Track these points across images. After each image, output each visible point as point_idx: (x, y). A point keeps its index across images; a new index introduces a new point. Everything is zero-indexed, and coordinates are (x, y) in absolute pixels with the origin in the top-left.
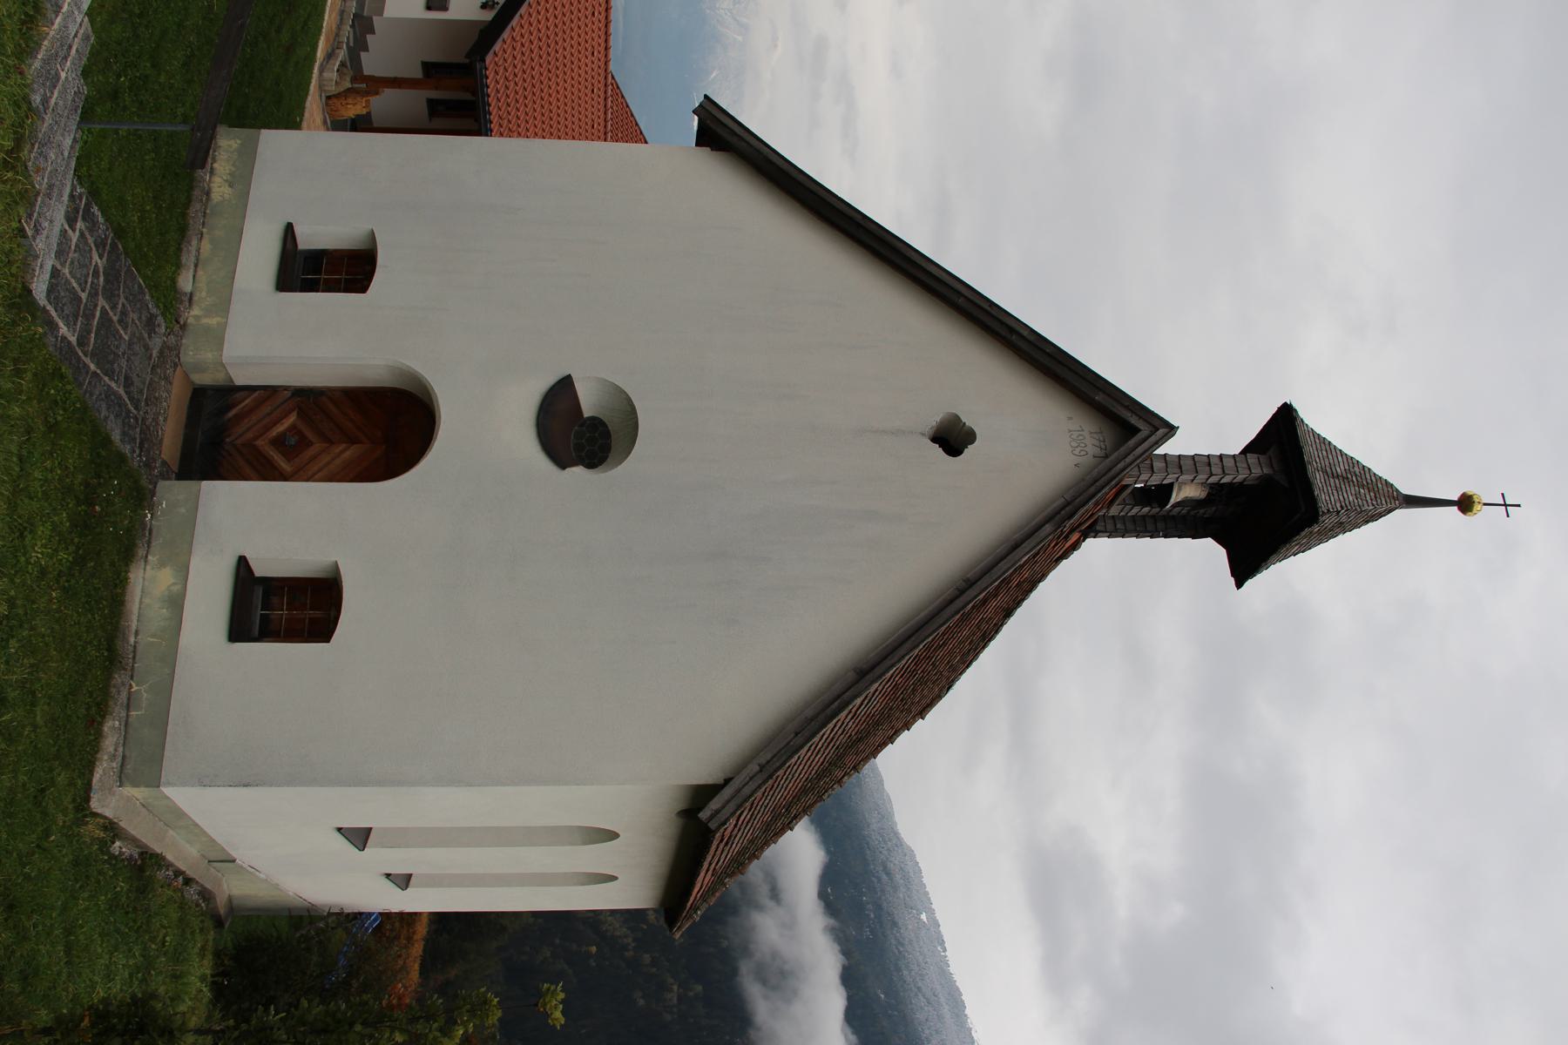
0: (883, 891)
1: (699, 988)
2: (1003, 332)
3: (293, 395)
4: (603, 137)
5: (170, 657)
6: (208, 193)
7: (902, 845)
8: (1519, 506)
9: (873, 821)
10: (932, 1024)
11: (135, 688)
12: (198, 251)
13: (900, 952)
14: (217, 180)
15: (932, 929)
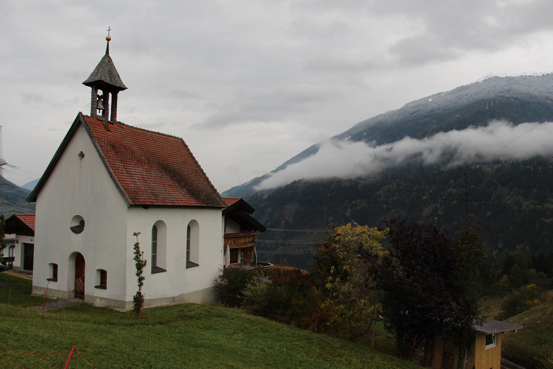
0: (420, 115)
1: (451, 181)
5: (109, 300)
6: (42, 295)
7: (404, 108)
9: (395, 118)
10: (469, 98)
11: (112, 306)
12: (51, 296)
13: (442, 109)
14: (40, 293)
15: (435, 97)
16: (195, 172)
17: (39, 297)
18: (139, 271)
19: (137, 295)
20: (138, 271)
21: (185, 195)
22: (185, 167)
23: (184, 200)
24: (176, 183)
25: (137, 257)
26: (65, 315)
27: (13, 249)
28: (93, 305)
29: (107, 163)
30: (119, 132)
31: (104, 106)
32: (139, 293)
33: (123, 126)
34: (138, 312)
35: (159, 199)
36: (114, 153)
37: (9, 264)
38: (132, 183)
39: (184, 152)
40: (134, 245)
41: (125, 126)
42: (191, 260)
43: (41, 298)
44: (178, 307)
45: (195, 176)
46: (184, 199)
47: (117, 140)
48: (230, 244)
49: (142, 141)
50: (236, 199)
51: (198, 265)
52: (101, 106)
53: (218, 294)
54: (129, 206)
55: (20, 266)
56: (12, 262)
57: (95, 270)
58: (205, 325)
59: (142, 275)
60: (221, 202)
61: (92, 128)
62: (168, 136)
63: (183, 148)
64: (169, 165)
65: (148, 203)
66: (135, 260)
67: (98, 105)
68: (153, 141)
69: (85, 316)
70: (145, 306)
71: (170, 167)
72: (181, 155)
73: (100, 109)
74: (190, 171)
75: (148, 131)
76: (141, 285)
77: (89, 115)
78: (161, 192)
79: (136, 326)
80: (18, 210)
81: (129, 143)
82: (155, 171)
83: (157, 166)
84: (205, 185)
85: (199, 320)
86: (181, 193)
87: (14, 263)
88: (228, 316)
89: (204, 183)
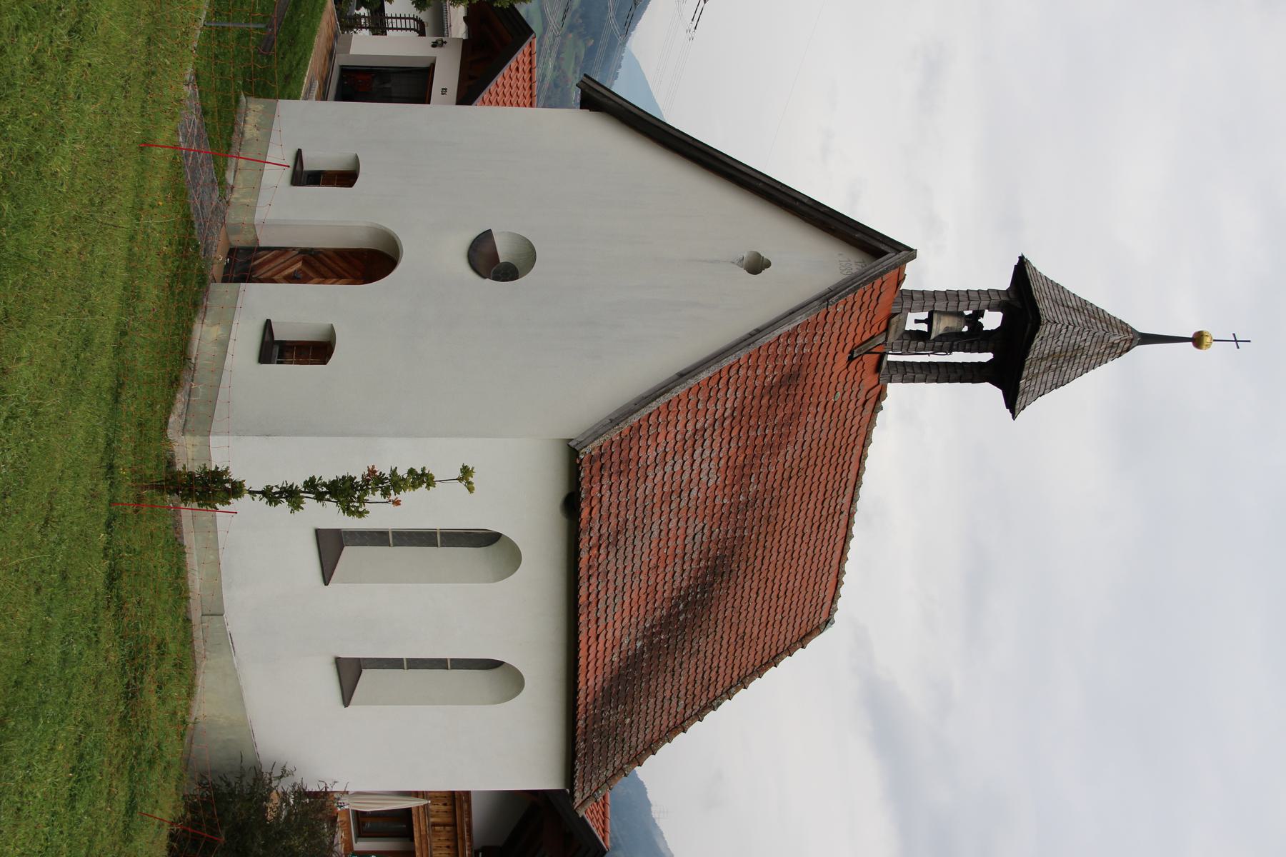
2: (789, 201)
3: (299, 253)
4: (527, 101)
5: (219, 370)
6: (243, 133)
8: (1249, 341)
16: (705, 682)
17: (234, 123)
18: (325, 489)
19: (228, 481)
20: (324, 484)
21: (617, 647)
22: (724, 642)
23: (601, 647)
24: (664, 612)
25: (380, 479)
26: (159, 224)
27: (414, 29)
28: (201, 315)
29: (732, 359)
30: (847, 394)
31: (941, 335)
32: (237, 490)
33: (869, 406)
34: (160, 488)
35: (602, 551)
36: (768, 380)
37: (360, 17)
38: (660, 449)
39: (782, 637)
40: (423, 469)
41: (870, 412)
42: (367, 675)
43: (233, 130)
44: (181, 634)
45: (691, 679)
46: (601, 645)
47: (816, 386)
48: (431, 807)
49: (815, 479)
50: (604, 830)
51: (347, 700)
52: (941, 325)
53: (229, 784)
54: (572, 444)
55: (351, 53)
56: (366, 28)
57: (330, 323)
58: (96, 753)
59: (309, 503)
60: (594, 784)
61: (858, 299)
62: (840, 572)
63: (796, 631)
64: (731, 583)
65: (584, 514)
66: (368, 475)
67: (946, 313)
68: (817, 518)
69: (152, 293)
70: (190, 515)
71: (723, 585)
72: (771, 623)
73: (929, 321)
74: (708, 660)
75: (853, 500)
76: (271, 496)
77: (904, 286)
78: (629, 558)
79: (103, 486)
80: (547, 42)
81: (808, 434)
82: (705, 531)
83: (725, 540)
84: (657, 722)
85: (121, 726)
86: (625, 631)
87: (366, 32)
88: (131, 841)
89: (665, 717)
